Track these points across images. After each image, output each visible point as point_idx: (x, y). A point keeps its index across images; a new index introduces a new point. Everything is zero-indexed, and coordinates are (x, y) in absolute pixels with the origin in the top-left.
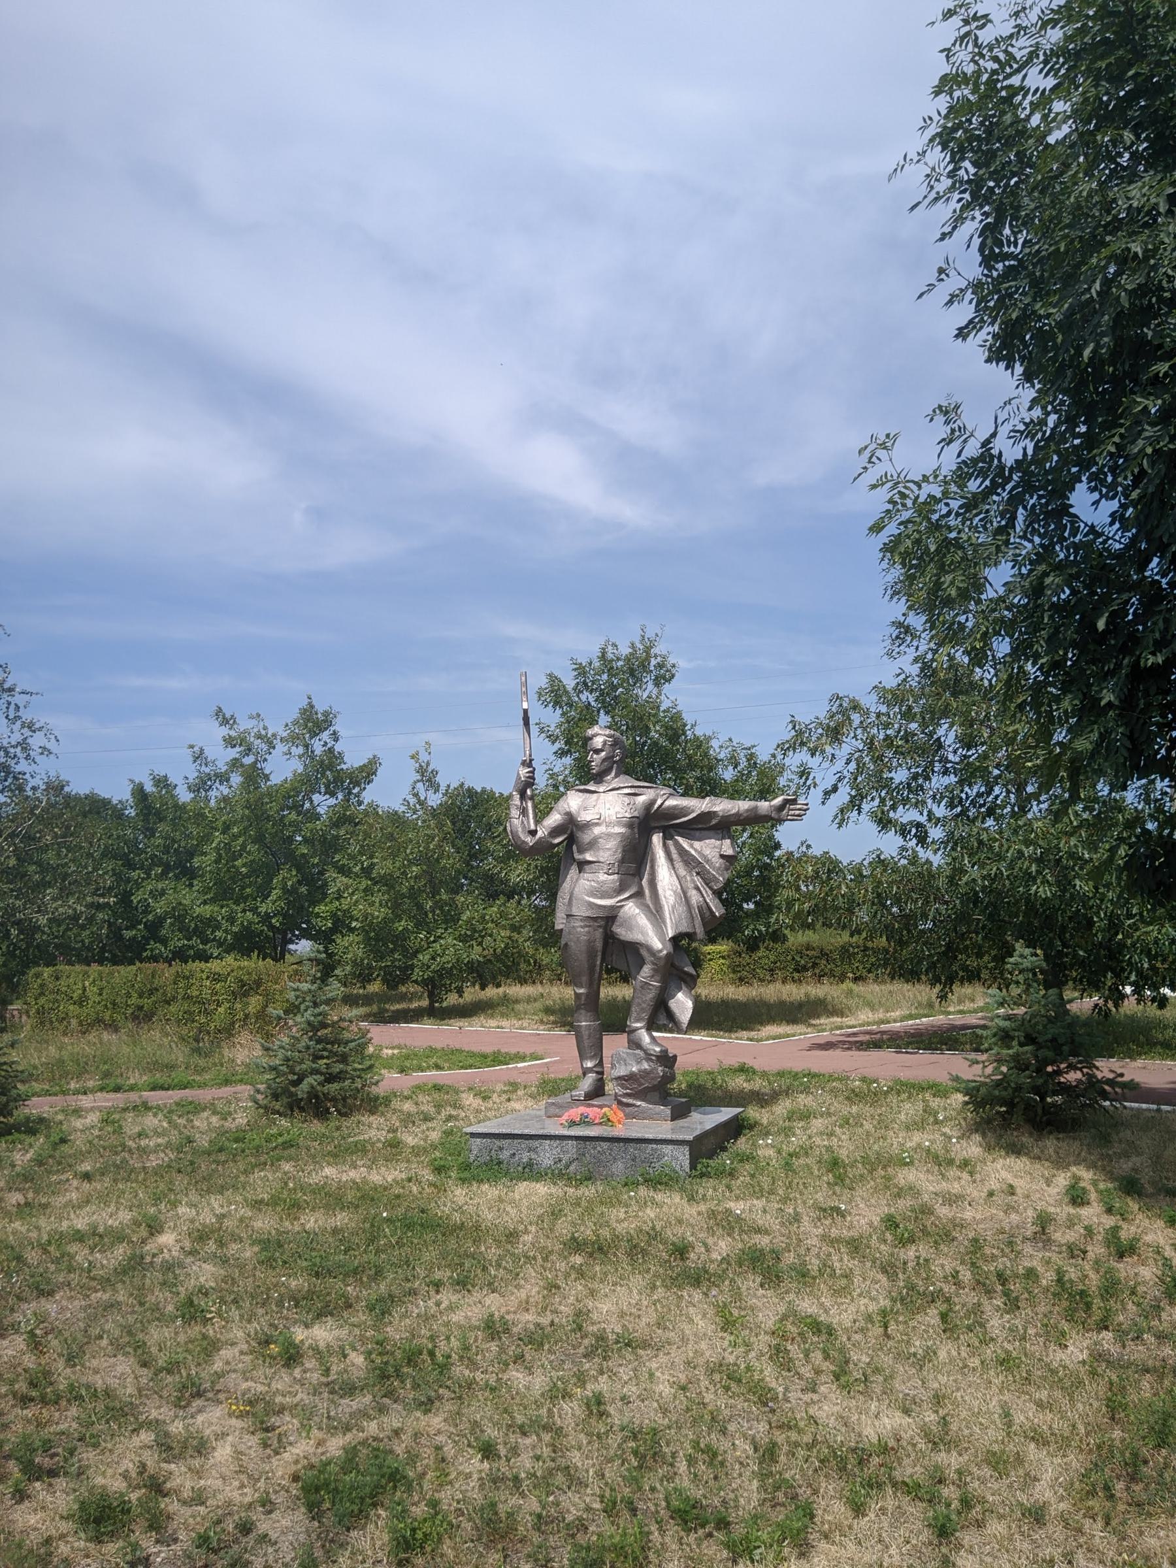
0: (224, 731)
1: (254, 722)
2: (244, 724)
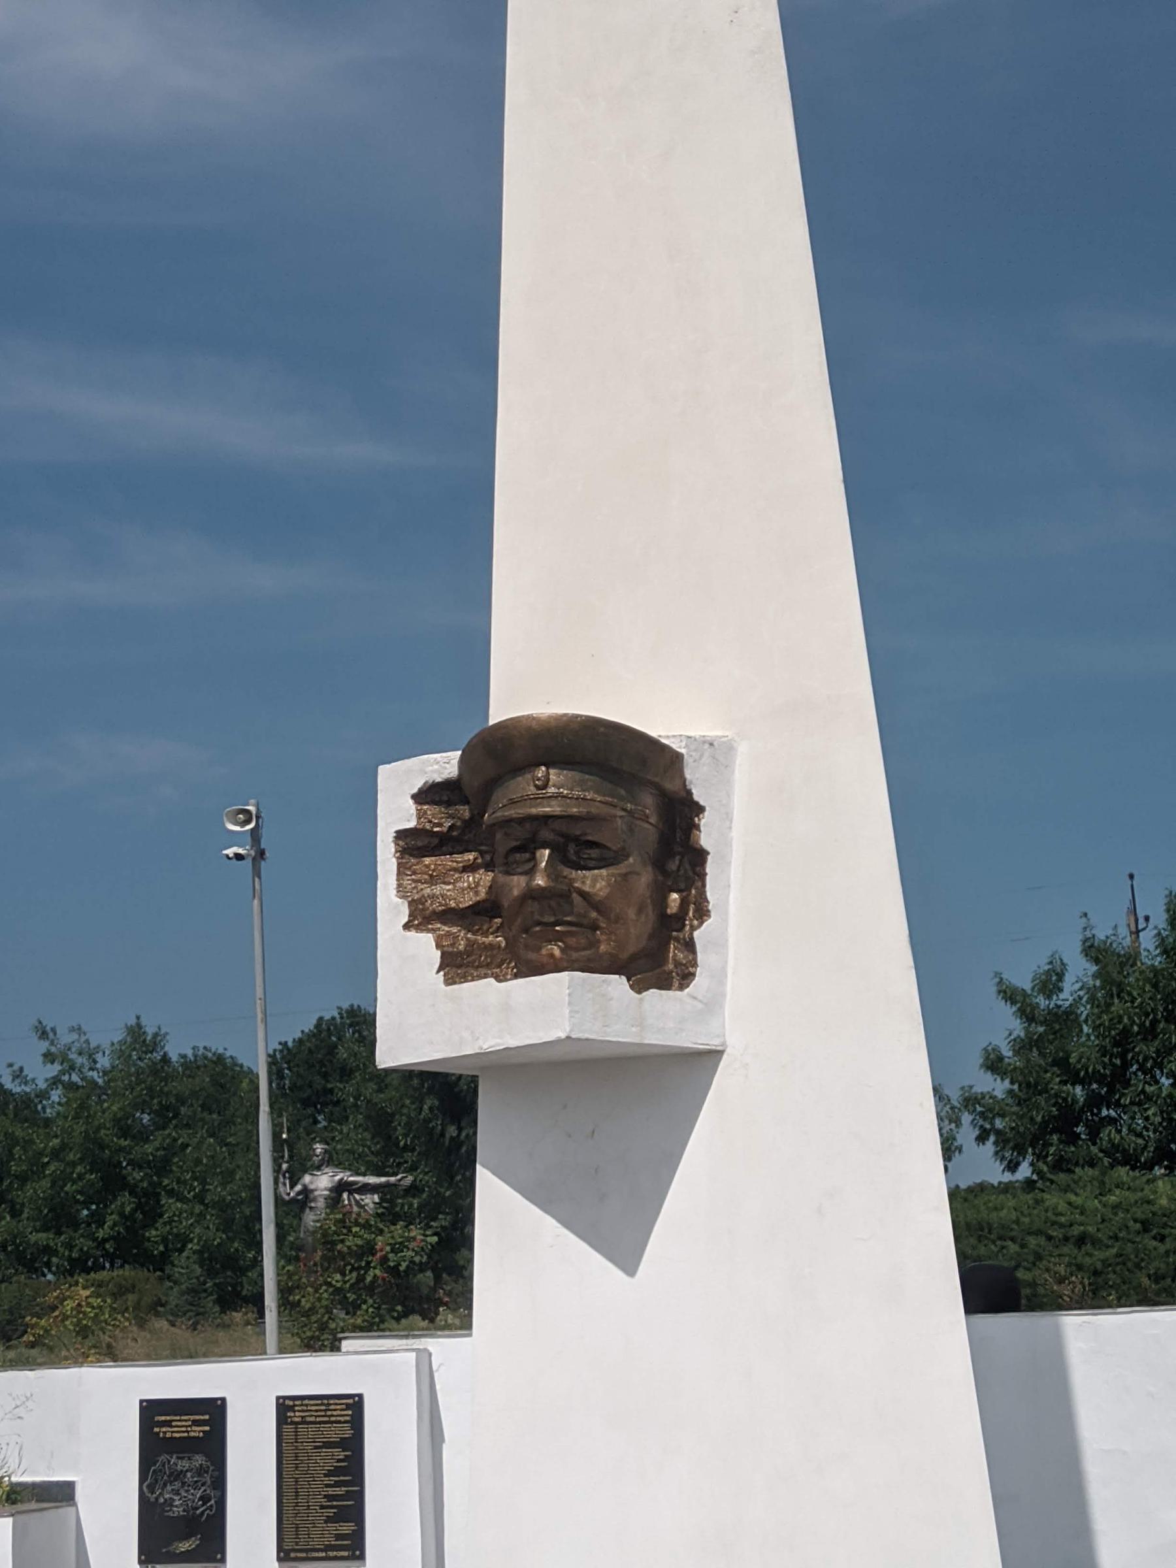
0: (44, 1046)
1: (75, 1036)
2: (65, 1038)
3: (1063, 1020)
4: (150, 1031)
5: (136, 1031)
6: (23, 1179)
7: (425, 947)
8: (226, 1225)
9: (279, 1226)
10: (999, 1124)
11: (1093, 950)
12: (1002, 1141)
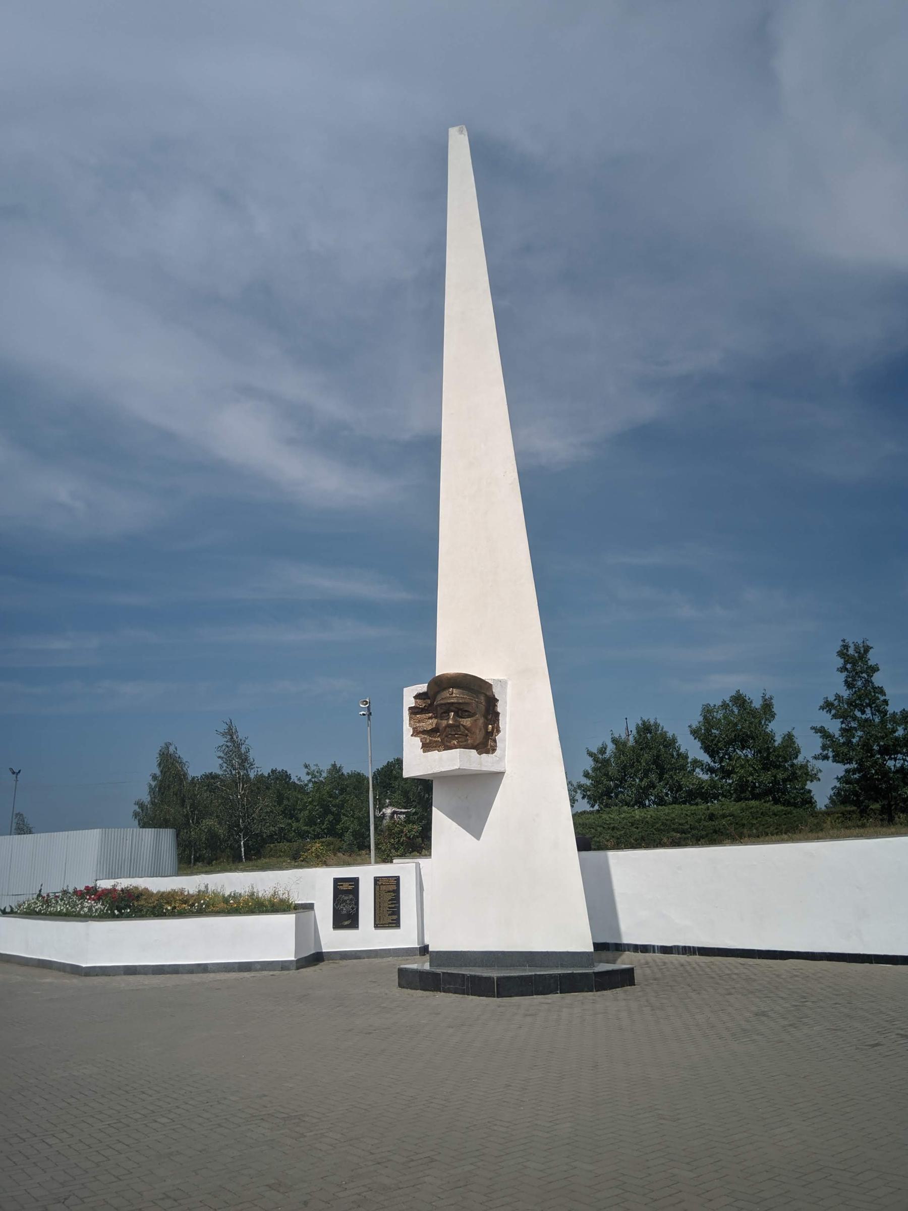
2: (313, 768)
3: (606, 762)
4: (338, 766)
5: (334, 766)
6: (301, 810)
7: (417, 741)
8: (360, 824)
9: (375, 824)
10: (588, 793)
11: (615, 741)
12: (589, 798)
